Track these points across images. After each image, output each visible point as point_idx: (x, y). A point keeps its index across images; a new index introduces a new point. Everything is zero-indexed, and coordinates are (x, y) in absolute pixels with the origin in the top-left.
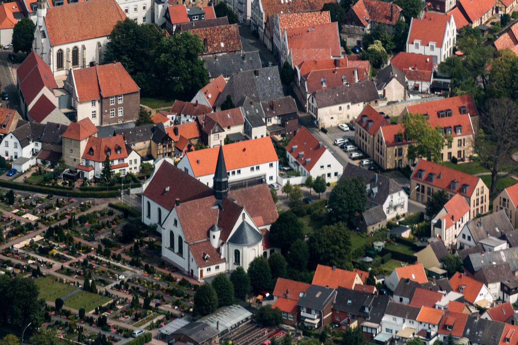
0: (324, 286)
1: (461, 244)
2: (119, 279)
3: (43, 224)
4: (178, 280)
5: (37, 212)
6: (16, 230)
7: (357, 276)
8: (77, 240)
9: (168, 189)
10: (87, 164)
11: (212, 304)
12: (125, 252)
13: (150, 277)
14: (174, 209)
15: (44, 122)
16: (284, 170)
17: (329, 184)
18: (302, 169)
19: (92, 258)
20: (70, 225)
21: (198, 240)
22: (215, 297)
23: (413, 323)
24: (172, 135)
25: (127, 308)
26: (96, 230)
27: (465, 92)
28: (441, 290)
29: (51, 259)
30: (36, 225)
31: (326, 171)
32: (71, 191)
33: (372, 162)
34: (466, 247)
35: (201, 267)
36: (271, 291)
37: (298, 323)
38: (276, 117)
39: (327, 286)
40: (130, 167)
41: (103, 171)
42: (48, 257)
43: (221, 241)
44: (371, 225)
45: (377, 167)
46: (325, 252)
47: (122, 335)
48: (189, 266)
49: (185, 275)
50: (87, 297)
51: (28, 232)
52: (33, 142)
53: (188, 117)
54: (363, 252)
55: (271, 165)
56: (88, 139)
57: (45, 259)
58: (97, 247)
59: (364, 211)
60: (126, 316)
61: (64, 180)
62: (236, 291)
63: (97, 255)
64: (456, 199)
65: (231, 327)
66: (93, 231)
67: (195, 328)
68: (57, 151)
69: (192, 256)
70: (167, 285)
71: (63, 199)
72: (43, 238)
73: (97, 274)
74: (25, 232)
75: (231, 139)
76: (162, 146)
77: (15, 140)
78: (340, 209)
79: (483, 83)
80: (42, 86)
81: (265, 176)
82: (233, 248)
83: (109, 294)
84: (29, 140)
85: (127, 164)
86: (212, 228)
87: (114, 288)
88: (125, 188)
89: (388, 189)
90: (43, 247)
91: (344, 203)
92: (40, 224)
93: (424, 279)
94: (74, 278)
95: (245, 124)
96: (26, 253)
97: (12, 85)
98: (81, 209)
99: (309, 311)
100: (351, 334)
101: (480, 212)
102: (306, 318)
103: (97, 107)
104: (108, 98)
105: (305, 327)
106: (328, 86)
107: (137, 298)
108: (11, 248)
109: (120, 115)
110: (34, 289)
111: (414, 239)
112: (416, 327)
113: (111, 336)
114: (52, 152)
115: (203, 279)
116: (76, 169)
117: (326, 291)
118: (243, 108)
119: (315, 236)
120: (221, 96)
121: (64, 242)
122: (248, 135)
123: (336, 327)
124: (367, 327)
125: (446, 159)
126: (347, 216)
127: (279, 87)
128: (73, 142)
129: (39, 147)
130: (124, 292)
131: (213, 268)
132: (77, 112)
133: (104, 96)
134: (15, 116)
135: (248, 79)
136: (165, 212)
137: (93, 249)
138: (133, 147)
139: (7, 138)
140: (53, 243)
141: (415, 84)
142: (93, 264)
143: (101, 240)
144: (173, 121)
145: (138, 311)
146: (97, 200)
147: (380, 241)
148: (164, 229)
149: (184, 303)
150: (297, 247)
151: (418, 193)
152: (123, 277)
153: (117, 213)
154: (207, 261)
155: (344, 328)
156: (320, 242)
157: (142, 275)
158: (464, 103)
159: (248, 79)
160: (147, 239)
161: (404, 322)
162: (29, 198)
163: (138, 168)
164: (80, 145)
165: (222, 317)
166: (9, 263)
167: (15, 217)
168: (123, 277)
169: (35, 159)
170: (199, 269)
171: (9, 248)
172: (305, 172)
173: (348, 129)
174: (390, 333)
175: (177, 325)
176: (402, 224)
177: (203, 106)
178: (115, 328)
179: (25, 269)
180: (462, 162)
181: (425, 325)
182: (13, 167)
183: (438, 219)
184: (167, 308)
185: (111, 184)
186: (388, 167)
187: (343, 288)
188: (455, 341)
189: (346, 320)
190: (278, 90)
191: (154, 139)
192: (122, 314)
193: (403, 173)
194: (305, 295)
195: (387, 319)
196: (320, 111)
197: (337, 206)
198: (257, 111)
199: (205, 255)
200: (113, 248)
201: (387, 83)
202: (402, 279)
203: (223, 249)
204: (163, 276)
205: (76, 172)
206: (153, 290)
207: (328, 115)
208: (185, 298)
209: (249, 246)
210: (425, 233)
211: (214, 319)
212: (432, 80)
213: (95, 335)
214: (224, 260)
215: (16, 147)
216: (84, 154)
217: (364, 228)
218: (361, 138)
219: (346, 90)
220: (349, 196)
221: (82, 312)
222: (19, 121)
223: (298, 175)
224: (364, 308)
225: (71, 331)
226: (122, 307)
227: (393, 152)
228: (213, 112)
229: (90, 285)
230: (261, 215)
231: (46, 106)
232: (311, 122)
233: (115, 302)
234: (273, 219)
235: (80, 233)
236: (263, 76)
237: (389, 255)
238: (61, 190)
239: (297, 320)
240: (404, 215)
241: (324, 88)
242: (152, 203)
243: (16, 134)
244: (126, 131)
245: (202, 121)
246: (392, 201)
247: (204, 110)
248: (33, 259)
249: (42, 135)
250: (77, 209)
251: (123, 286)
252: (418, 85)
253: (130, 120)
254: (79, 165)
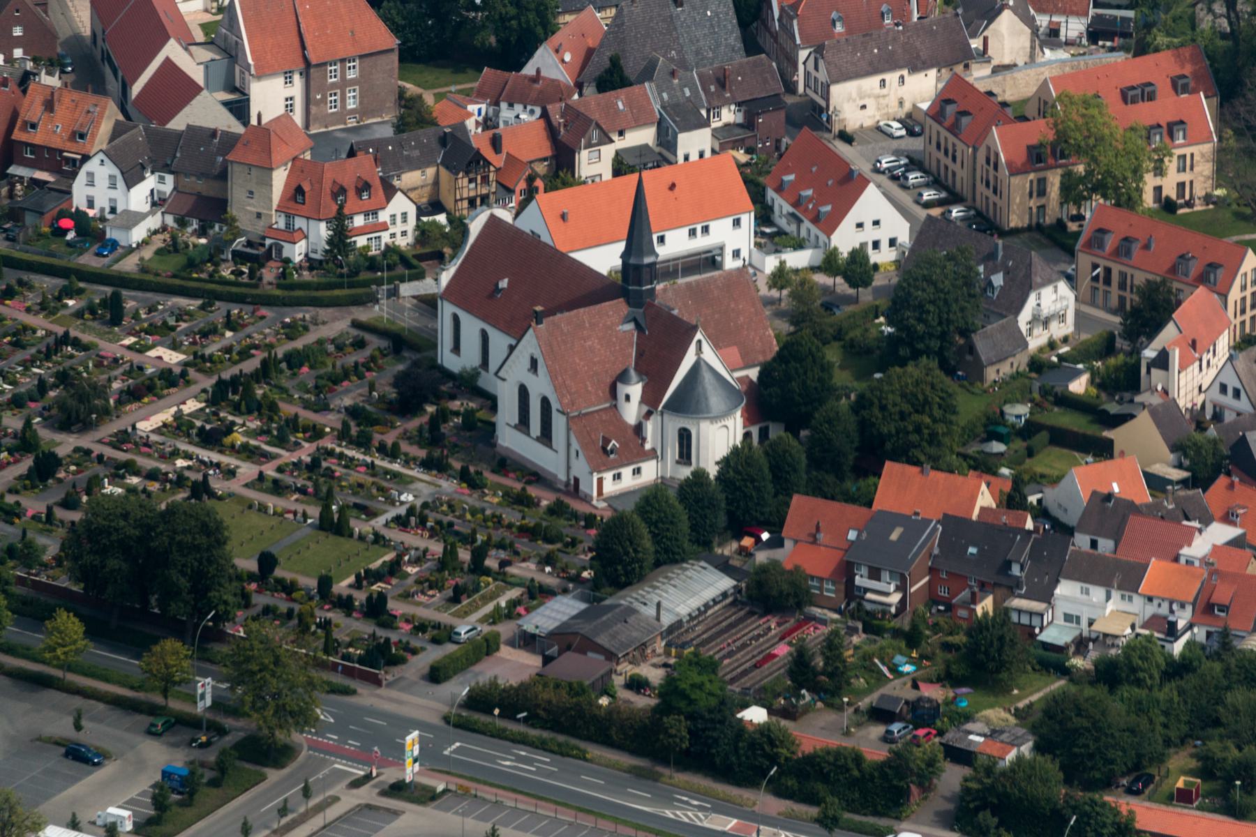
1: (1215, 407)
2: (402, 503)
3: (199, 370)
4: (544, 503)
5: (181, 343)
6: (136, 386)
7: (984, 487)
8: (287, 409)
9: (504, 284)
10: (288, 225)
11: (640, 561)
12: (406, 436)
13: (475, 496)
14: (531, 331)
15: (178, 123)
16: (763, 234)
17: (876, 267)
18: (809, 231)
19: (330, 453)
20: (265, 372)
21: (589, 406)
22: (647, 543)
23: (1130, 599)
24: (488, 152)
25: (432, 571)
26: (330, 384)
27: (1175, 40)
28: (1188, 519)
29: (230, 455)
30: (184, 374)
31: (869, 235)
32: (254, 292)
33: (972, 212)
34: (1229, 417)
35: (599, 472)
36: (776, 526)
37: (848, 604)
38: (733, 107)
39: (917, 514)
40: (391, 231)
41: (330, 242)
42: (221, 452)
43: (645, 409)
44: (992, 364)
45: (985, 222)
46: (898, 433)
47: (427, 636)
48: (569, 468)
49: (559, 490)
50: (329, 546)
51: (165, 392)
52: (153, 173)
53: (518, 108)
54: (980, 429)
55: (737, 223)
56: (289, 165)
57: (215, 457)
58: (339, 426)
59: (974, 331)
60: (431, 593)
61: (236, 264)
62: (693, 528)
63: (340, 446)
64: (1196, 301)
65: (690, 615)
66: (324, 386)
67: (604, 618)
68: (212, 194)
69: (575, 445)
70: (519, 515)
71: (241, 310)
72: (203, 405)
73: (346, 491)
74: (158, 391)
75: (629, 160)
76: (466, 180)
77: (110, 169)
78: (920, 328)
79: (1228, 18)
80: (166, 38)
81: (722, 248)
82: (674, 424)
83: (384, 538)
84: (143, 168)
85: (385, 223)
86: (623, 377)
87: (392, 525)
88: (390, 281)
89: (1028, 276)
90: (208, 427)
91: (929, 312)
92: (192, 372)
93: (1143, 496)
94: (291, 502)
95: (661, 124)
96: (170, 441)
97: (77, 38)
98: (286, 334)
99: (875, 574)
100: (988, 630)
101: (1248, 330)
102: (866, 590)
103: (297, 89)
104: (325, 64)
105: (868, 613)
106: (849, 30)
107: (453, 546)
108: (130, 430)
109: (351, 105)
110: (217, 528)
111: (1098, 397)
112: (1139, 608)
113: (400, 641)
114: (200, 198)
115: (605, 500)
116: (264, 238)
117: (914, 526)
118: (653, 85)
119: (872, 391)
120: (595, 58)
121: (256, 414)
122: (668, 149)
123: (939, 611)
124: (1020, 611)
125: (1148, 199)
126: (935, 344)
127: (732, 36)
128: (254, 171)
129: (168, 185)
130: (416, 534)
131: (627, 472)
132: (248, 100)
133: (314, 61)
134: (107, 113)
135: (660, 15)
136: (499, 341)
137: (328, 430)
138: (396, 183)
139: (92, 165)
140: (230, 418)
141: (1050, 22)
142: (333, 467)
143: (346, 409)
144: (480, 119)
145: (460, 577)
146: (324, 313)
147: (1018, 402)
148: (504, 380)
149: (565, 559)
150: (829, 422)
151: (1096, 285)
152: (411, 498)
153: (375, 342)
154: (612, 456)
155: (963, 613)
156: (883, 408)
157: (456, 492)
158: (1183, 66)
159: (660, 15)
160: (456, 405)
161: (1108, 598)
162: (156, 310)
163: (410, 234)
164: (271, 179)
165: (667, 592)
166: (131, 468)
167: (129, 356)
168: (411, 498)
169: (159, 214)
170: (596, 477)
171: (126, 431)
172: (817, 237)
173: (903, 132)
174: (1074, 625)
175: (558, 612)
176: (1066, 361)
177: (553, 81)
178: (407, 621)
179: (171, 481)
180: (1186, 210)
181: (1159, 605)
182: (108, 236)
183: (1160, 348)
184: (525, 570)
185: (349, 273)
186: (1012, 225)
187: (955, 517)
188: (1235, 643)
189: (965, 594)
190: (732, 41)
191: (446, 164)
192: (420, 587)
193: (1056, 240)
194: (864, 535)
195: (1066, 589)
196: (836, 90)
197: (912, 321)
198: (688, 93)
199: (606, 441)
200: (377, 428)
201: (991, 20)
202: (1094, 493)
203: (650, 428)
204: (507, 494)
205: (263, 245)
206: (487, 527)
207: (854, 101)
208: (567, 545)
209: (714, 419)
210: (1126, 381)
211: (648, 596)
212: (1092, 12)
213: (363, 639)
214: (652, 455)
215: (113, 186)
216: (281, 201)
217: (977, 371)
218: (941, 155)
219: (894, 39)
220: (942, 296)
221: (325, 583)
222: (117, 123)
223: (799, 245)
224: (1008, 565)
225: (303, 628)
226: (416, 570)
227: (1024, 186)
228: (576, 97)
229: (336, 517)
230: (735, 344)
231: (175, 88)
232: (814, 116)
233: (400, 557)
234: (764, 352)
235: (291, 392)
236: (694, 8)
237: (1044, 436)
238: (234, 289)
239: (846, 596)
240: (1065, 340)
241: (839, 34)
242: (464, 317)
243: (113, 155)
244: (379, 145)
245: (557, 119)
246: (1039, 305)
247: (554, 91)
248: (188, 456)
249: (175, 156)
250: (277, 333)
251: (413, 519)
252: (1059, 24)
253: (373, 117)
254: (270, 227)
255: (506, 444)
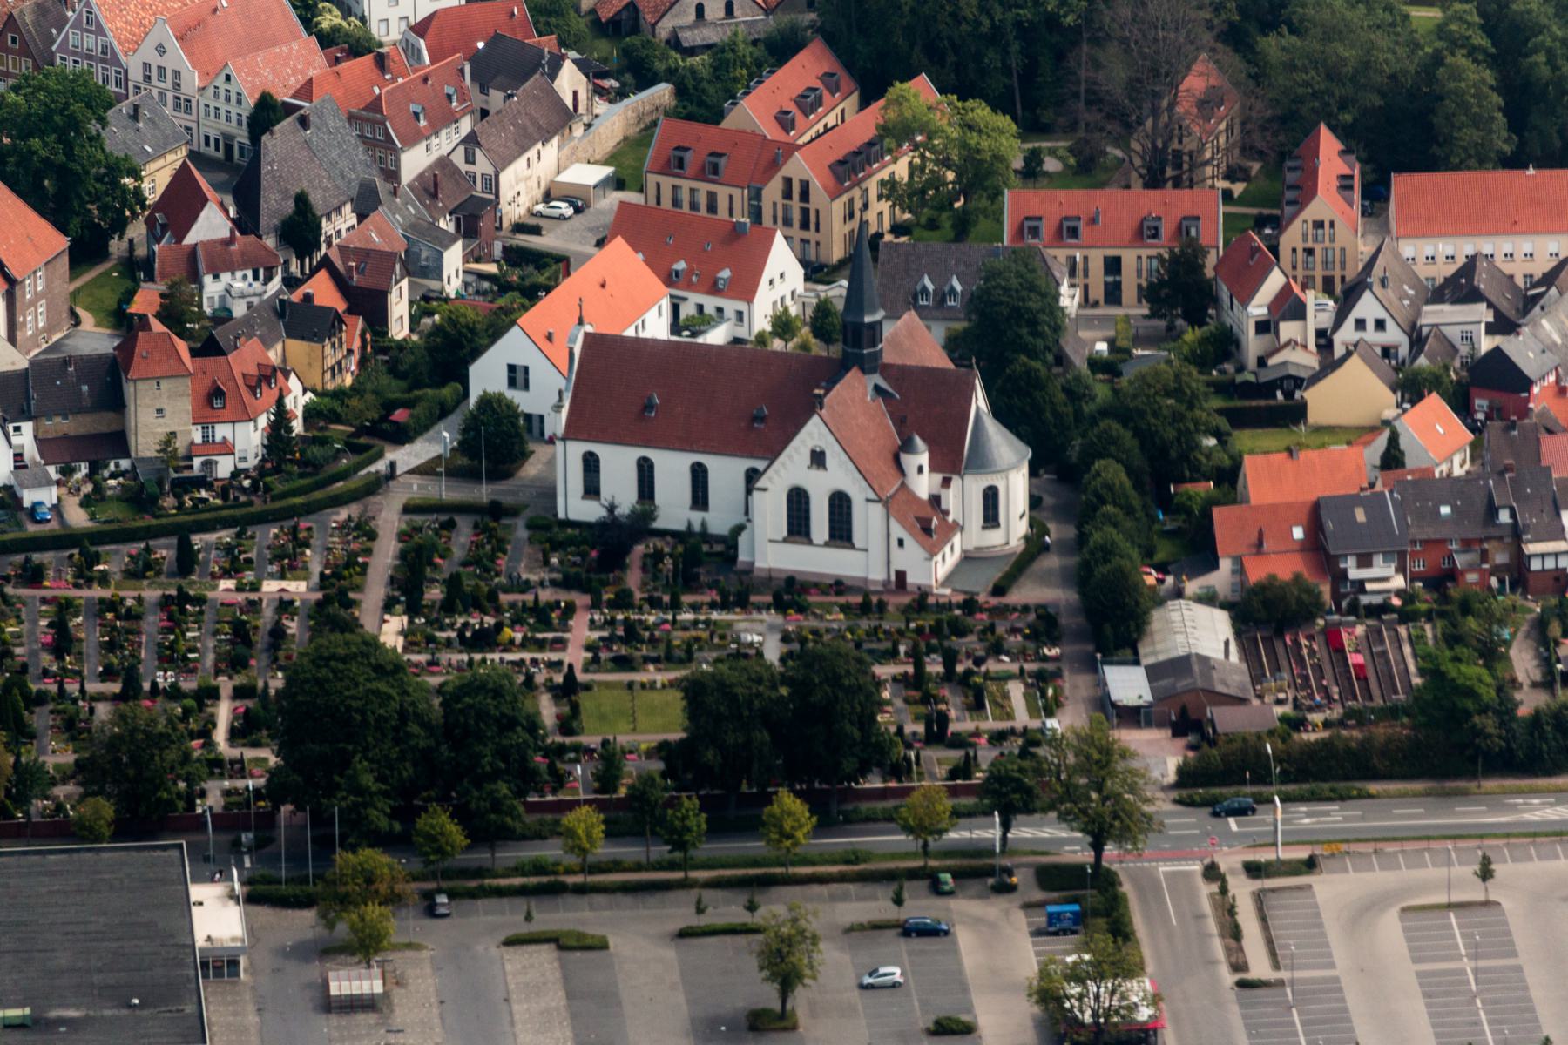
0: (1355, 491)
68: (82, 431)
124: (1543, 556)
148: (764, 490)
255: (765, 565)
